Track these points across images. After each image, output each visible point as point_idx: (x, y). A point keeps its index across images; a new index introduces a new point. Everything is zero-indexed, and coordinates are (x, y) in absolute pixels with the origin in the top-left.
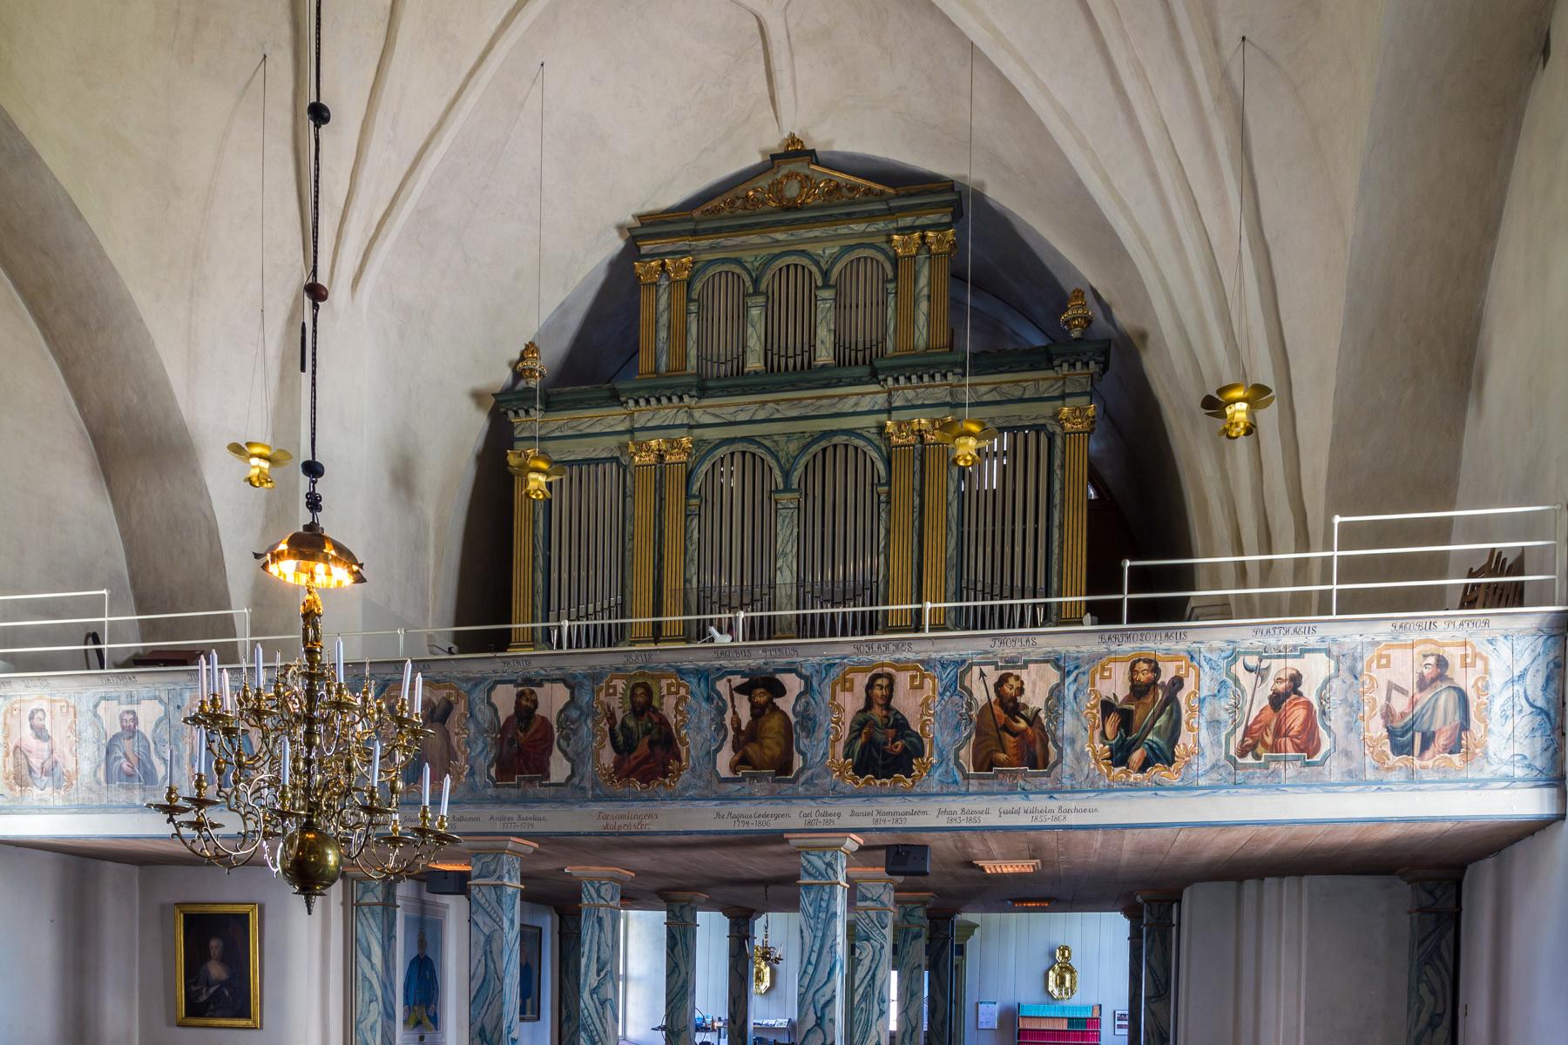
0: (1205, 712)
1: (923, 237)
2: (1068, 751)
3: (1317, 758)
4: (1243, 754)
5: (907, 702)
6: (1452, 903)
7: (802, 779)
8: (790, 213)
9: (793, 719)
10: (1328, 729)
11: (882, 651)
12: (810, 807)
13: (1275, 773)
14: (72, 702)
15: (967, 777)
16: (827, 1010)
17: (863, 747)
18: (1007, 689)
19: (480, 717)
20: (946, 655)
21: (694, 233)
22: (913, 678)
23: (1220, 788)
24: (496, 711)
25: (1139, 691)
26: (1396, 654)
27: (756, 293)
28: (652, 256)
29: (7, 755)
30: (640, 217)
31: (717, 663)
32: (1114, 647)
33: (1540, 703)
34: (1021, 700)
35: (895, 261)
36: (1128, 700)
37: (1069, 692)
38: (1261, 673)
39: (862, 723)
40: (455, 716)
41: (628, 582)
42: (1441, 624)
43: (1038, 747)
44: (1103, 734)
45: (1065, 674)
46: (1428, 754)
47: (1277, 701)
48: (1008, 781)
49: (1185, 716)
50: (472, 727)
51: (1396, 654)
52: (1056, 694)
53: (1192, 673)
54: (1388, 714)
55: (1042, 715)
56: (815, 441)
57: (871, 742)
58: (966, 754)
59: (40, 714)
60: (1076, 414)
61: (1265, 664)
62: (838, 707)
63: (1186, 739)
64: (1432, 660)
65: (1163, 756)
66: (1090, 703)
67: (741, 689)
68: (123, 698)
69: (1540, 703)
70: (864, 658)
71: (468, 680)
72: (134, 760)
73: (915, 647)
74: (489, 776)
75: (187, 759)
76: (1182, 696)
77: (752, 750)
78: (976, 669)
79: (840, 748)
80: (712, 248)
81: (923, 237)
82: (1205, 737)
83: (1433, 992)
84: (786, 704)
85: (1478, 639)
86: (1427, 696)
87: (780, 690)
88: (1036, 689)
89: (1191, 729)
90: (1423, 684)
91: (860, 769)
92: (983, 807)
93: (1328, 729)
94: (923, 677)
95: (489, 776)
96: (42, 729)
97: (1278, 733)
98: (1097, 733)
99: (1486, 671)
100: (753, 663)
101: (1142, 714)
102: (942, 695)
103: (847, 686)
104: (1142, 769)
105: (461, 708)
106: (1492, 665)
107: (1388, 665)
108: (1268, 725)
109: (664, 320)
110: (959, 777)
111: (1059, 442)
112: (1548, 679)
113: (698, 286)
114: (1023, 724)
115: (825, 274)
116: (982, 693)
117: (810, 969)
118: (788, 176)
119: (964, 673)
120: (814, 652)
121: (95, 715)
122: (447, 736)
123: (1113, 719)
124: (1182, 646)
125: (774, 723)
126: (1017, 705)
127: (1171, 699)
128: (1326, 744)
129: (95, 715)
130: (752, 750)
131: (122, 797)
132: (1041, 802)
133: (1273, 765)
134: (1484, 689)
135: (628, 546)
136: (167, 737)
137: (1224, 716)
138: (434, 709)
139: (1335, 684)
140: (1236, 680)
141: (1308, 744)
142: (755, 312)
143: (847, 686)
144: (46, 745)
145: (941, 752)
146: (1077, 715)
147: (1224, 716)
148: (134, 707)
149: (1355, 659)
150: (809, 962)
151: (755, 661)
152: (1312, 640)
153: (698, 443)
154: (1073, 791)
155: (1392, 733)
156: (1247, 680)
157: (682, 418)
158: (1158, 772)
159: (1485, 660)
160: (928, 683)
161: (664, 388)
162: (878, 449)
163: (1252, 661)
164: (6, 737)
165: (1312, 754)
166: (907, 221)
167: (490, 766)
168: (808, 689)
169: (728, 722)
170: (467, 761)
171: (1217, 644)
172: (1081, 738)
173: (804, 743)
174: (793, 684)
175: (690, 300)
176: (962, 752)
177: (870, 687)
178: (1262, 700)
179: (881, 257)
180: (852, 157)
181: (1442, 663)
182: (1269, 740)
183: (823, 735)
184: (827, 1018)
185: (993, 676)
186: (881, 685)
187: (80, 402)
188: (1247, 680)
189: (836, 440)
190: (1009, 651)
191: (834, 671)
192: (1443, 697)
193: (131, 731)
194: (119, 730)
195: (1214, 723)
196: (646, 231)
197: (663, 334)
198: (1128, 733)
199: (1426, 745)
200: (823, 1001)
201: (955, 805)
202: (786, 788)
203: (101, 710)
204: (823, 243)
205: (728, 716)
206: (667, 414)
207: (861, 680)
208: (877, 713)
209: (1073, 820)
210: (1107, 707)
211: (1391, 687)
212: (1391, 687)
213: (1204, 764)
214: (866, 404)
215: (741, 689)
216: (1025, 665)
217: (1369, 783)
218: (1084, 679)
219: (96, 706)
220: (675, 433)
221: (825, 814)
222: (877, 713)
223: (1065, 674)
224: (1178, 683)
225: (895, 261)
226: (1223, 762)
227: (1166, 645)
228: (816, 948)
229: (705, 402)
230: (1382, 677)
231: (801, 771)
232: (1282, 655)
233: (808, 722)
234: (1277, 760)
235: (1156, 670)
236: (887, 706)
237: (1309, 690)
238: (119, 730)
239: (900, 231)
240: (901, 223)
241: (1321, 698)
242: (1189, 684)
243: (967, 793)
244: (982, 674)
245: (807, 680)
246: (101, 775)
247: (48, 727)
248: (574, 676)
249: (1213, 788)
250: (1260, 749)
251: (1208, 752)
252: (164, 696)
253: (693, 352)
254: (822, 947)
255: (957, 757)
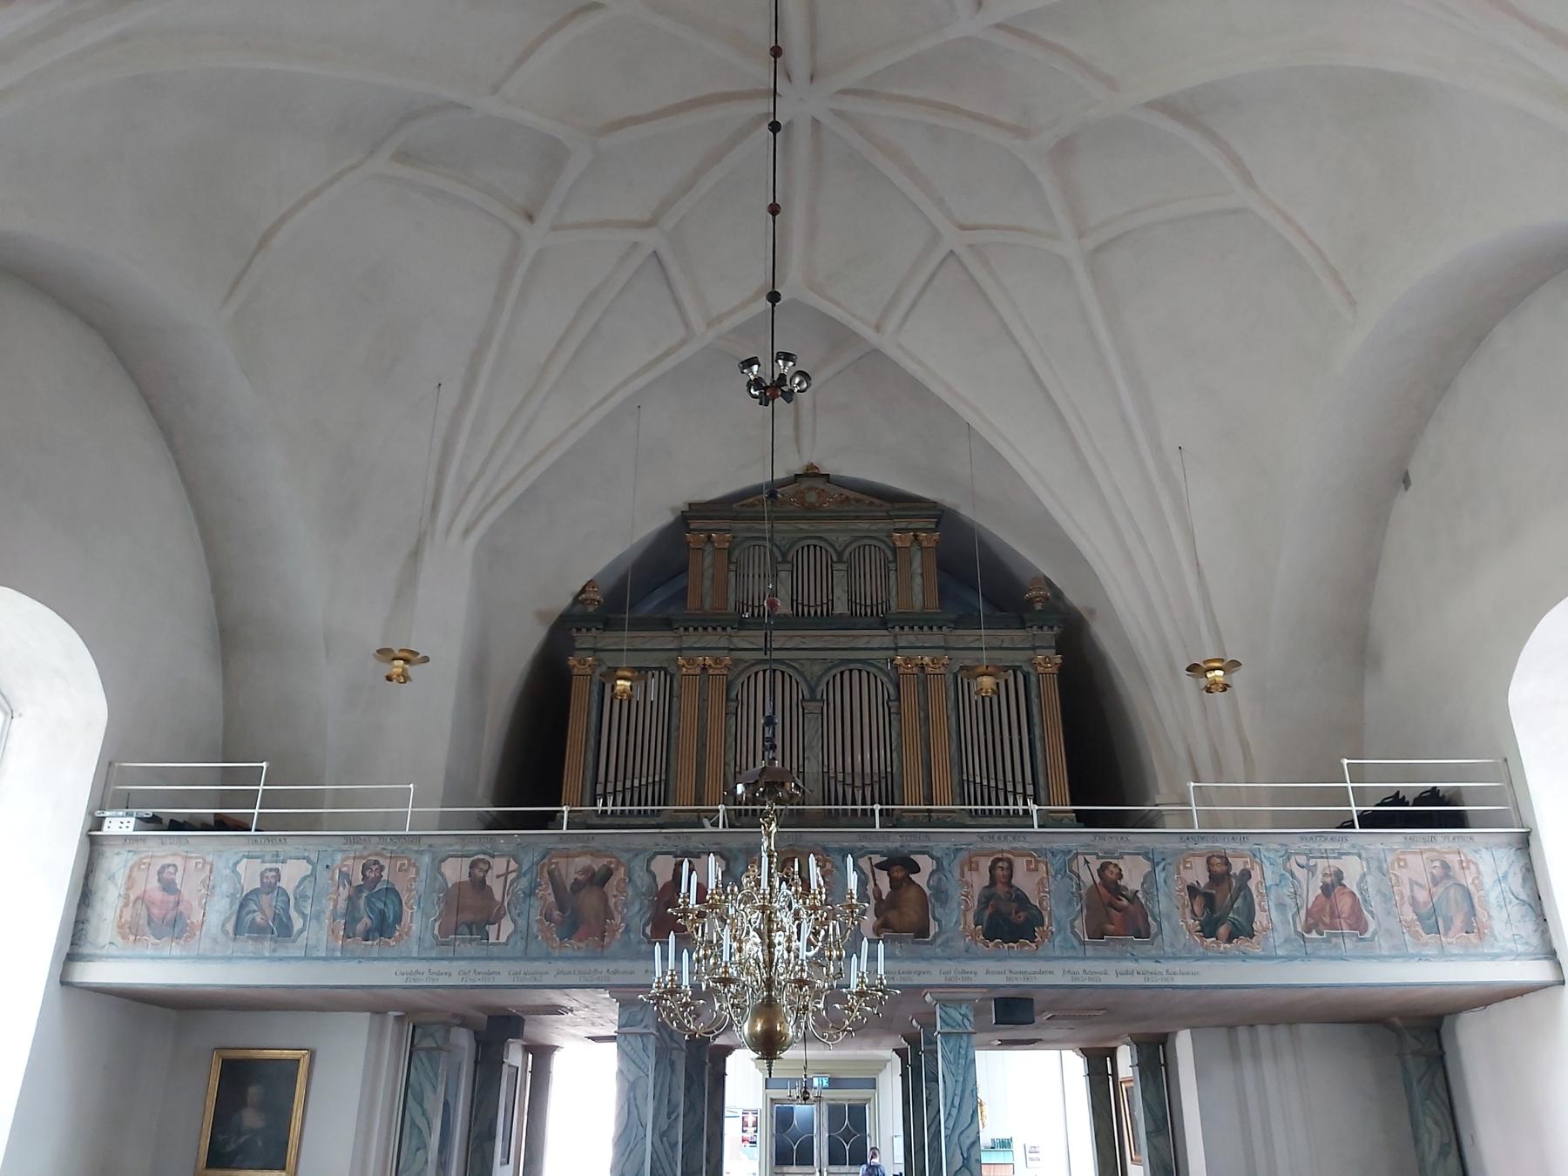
0: (1272, 897)
1: (916, 536)
2: (1165, 924)
3: (1367, 936)
4: (1309, 932)
5: (1023, 879)
6: (1436, 1047)
7: (939, 941)
8: (810, 512)
9: (928, 892)
10: (1371, 913)
11: (1000, 840)
12: (950, 965)
13: (1336, 945)
14: (209, 859)
15: (1084, 943)
16: (973, 1152)
17: (990, 916)
18: (1107, 873)
19: (639, 882)
20: (1055, 846)
21: (734, 518)
22: (1029, 863)
23: (1296, 958)
24: (654, 877)
25: (1218, 878)
26: (1410, 859)
27: (785, 561)
28: (701, 531)
29: (126, 905)
30: (690, 505)
31: (859, 844)
32: (1191, 846)
33: (1523, 897)
34: (1121, 883)
35: (894, 550)
36: (1208, 886)
37: (1160, 876)
38: (1312, 870)
39: (987, 898)
40: (614, 881)
41: (672, 762)
42: (1439, 838)
43: (1140, 919)
44: (1193, 911)
45: (1155, 865)
46: (1451, 933)
47: (1327, 890)
48: (1118, 947)
49: (1256, 901)
50: (630, 892)
51: (1410, 859)
52: (1149, 879)
53: (1257, 868)
54: (1414, 902)
55: (1140, 895)
56: (835, 666)
57: (996, 913)
58: (1080, 925)
59: (171, 869)
60: (1048, 661)
61: (1312, 862)
62: (967, 883)
63: (1260, 919)
64: (1437, 864)
65: (1242, 930)
66: (1178, 886)
67: (880, 866)
68: (268, 858)
69: (1523, 897)
70: (987, 845)
71: (628, 850)
72: (270, 915)
73: (1029, 838)
74: (644, 934)
75: (328, 914)
76: (1252, 884)
77: (892, 916)
78: (1081, 858)
79: (970, 917)
80: (749, 530)
81: (916, 536)
82: (1274, 915)
83: (1436, 1123)
84: (920, 879)
85: (1468, 852)
86: (1440, 889)
87: (917, 870)
88: (1133, 876)
89: (1263, 910)
90: (1436, 882)
91: (990, 935)
92: (1101, 969)
93: (1371, 913)
94: (1037, 862)
95: (644, 934)
96: (173, 882)
97: (1332, 915)
98: (1188, 911)
99: (1478, 872)
100: (891, 845)
101: (1222, 899)
102: (1054, 877)
103: (974, 867)
104: (1229, 941)
105: (621, 873)
106: (1482, 867)
107: (1406, 866)
108: (1323, 909)
109: (708, 574)
110: (1076, 943)
111: (1033, 679)
112: (1524, 880)
113: (736, 553)
114: (1125, 902)
115: (840, 554)
116: (1088, 876)
117: (954, 1112)
118: (810, 489)
119: (1071, 860)
120: (944, 839)
121: (234, 871)
122: (605, 900)
123: (1199, 901)
124: (1246, 847)
125: (912, 893)
126: (1118, 887)
127: (1243, 887)
128: (1372, 926)
129: (234, 871)
130: (892, 916)
131: (250, 947)
132: (1150, 966)
133: (1334, 940)
134: (1480, 887)
135: (674, 734)
136: (310, 894)
137: (1289, 901)
138: (594, 874)
139: (1369, 879)
140: (1292, 874)
141: (1359, 924)
142: (783, 574)
143: (974, 867)
144: (172, 898)
145: (1058, 923)
146: (1169, 896)
147: (1289, 901)
148: (279, 866)
149: (1379, 861)
150: (952, 1105)
151: (894, 844)
152: (1346, 846)
153: (736, 662)
154: (1175, 958)
155: (1420, 918)
156: (1301, 874)
157: (724, 643)
158: (1241, 944)
159: (1476, 864)
160: (1042, 867)
161: (706, 623)
162: (887, 674)
163: (1302, 860)
164: (128, 889)
165: (1365, 930)
166: (903, 525)
167: (646, 924)
168: (939, 868)
169: (870, 892)
170: (623, 920)
171: (1272, 846)
172: (1174, 916)
173: (939, 912)
174: (925, 863)
175: (730, 562)
176: (1077, 923)
177: (992, 869)
178: (1315, 891)
179: (883, 546)
180: (855, 481)
181: (1446, 866)
182: (1327, 920)
183: (954, 905)
184: (973, 1159)
185: (1096, 865)
186: (1002, 870)
187: (219, 605)
188: (1301, 874)
189: (852, 666)
190: (1108, 845)
191: (963, 855)
192: (1452, 891)
193: (271, 885)
194: (258, 885)
195: (1281, 906)
196: (693, 515)
197: (707, 583)
198: (1213, 911)
199: (1448, 929)
200: (968, 1142)
201: (1078, 966)
202: (925, 950)
203: (241, 868)
204: (838, 534)
205: (870, 887)
206: (711, 639)
207: (985, 863)
208: (1001, 889)
209: (1179, 981)
210: (1193, 890)
211: (1412, 883)
212: (1412, 883)
213: (1278, 938)
214: (875, 643)
215: (880, 866)
216: (1121, 857)
217: (1412, 957)
218: (1171, 868)
219: (236, 864)
220: (718, 653)
221: (964, 972)
222: (1001, 889)
223: (1155, 865)
224: (1246, 874)
225: (894, 550)
226: (1293, 936)
227: (1233, 845)
228: (958, 1092)
229: (743, 633)
230: (1404, 875)
231: (937, 935)
232: (1325, 855)
233: (941, 894)
234: (1336, 935)
235: (1227, 863)
236: (1009, 885)
237: (1351, 882)
238: (258, 885)
239: (896, 530)
240: (897, 526)
241: (1360, 890)
242: (1256, 874)
243: (1085, 958)
244: (1087, 862)
245: (938, 861)
246: (230, 927)
247: (178, 881)
248: (730, 850)
249: (1290, 958)
250: (1321, 926)
251: (1279, 927)
252: (314, 857)
253: (732, 598)
254: (963, 1091)
255: (1073, 927)
